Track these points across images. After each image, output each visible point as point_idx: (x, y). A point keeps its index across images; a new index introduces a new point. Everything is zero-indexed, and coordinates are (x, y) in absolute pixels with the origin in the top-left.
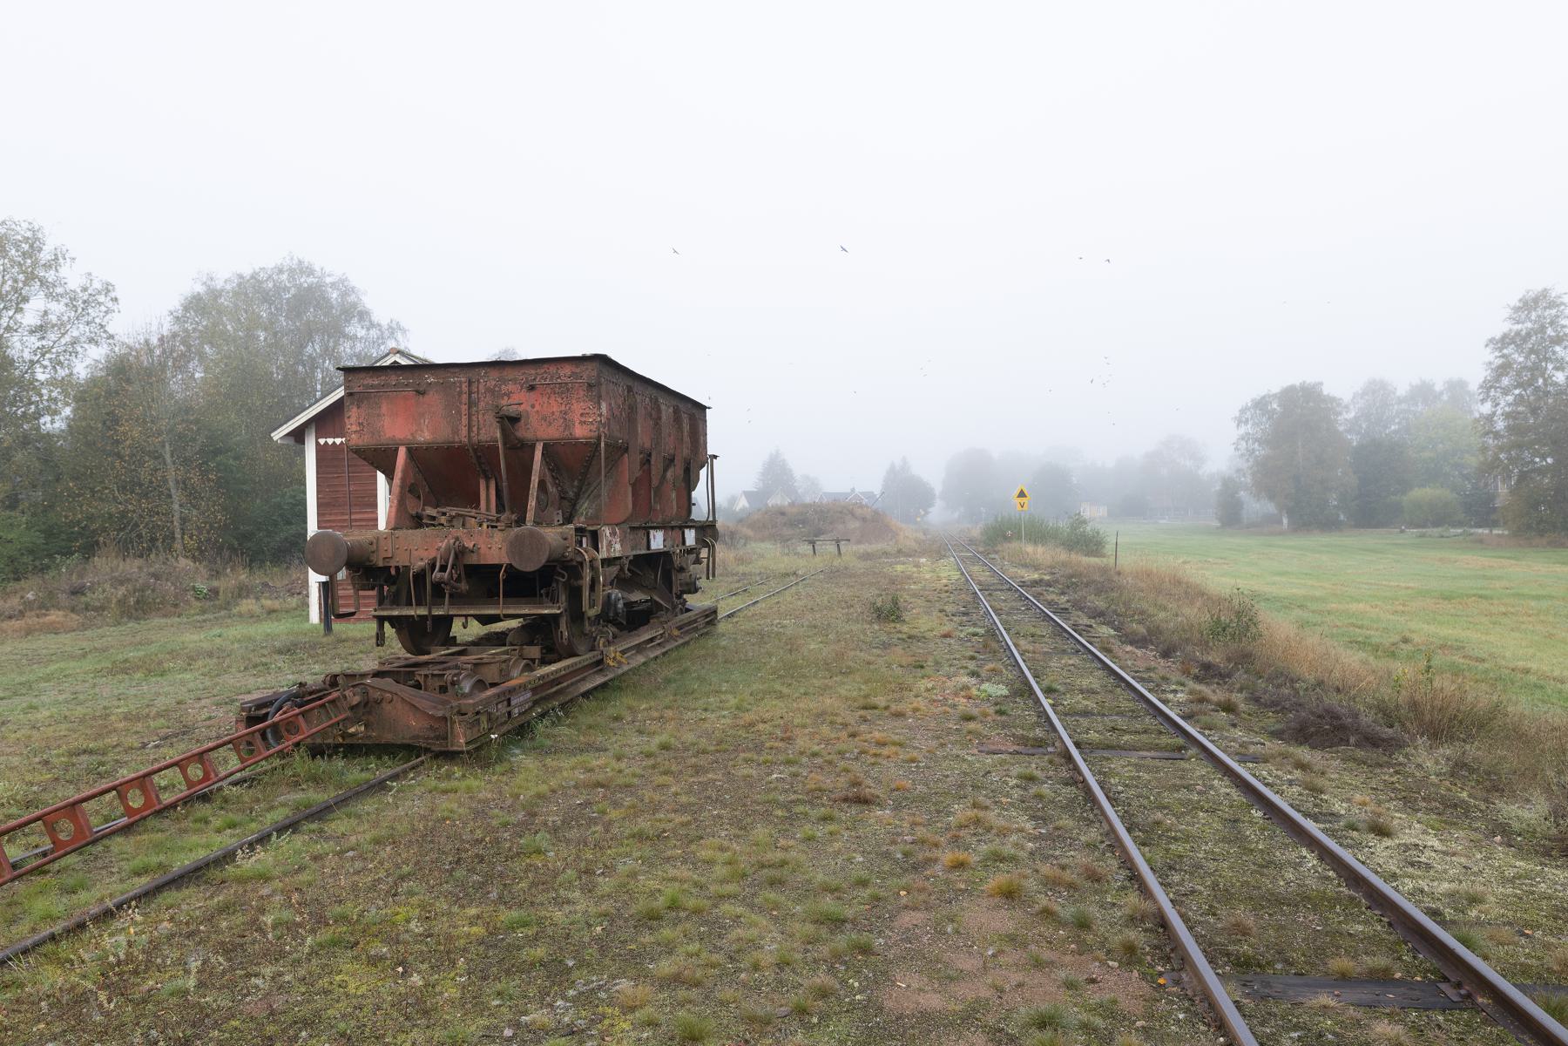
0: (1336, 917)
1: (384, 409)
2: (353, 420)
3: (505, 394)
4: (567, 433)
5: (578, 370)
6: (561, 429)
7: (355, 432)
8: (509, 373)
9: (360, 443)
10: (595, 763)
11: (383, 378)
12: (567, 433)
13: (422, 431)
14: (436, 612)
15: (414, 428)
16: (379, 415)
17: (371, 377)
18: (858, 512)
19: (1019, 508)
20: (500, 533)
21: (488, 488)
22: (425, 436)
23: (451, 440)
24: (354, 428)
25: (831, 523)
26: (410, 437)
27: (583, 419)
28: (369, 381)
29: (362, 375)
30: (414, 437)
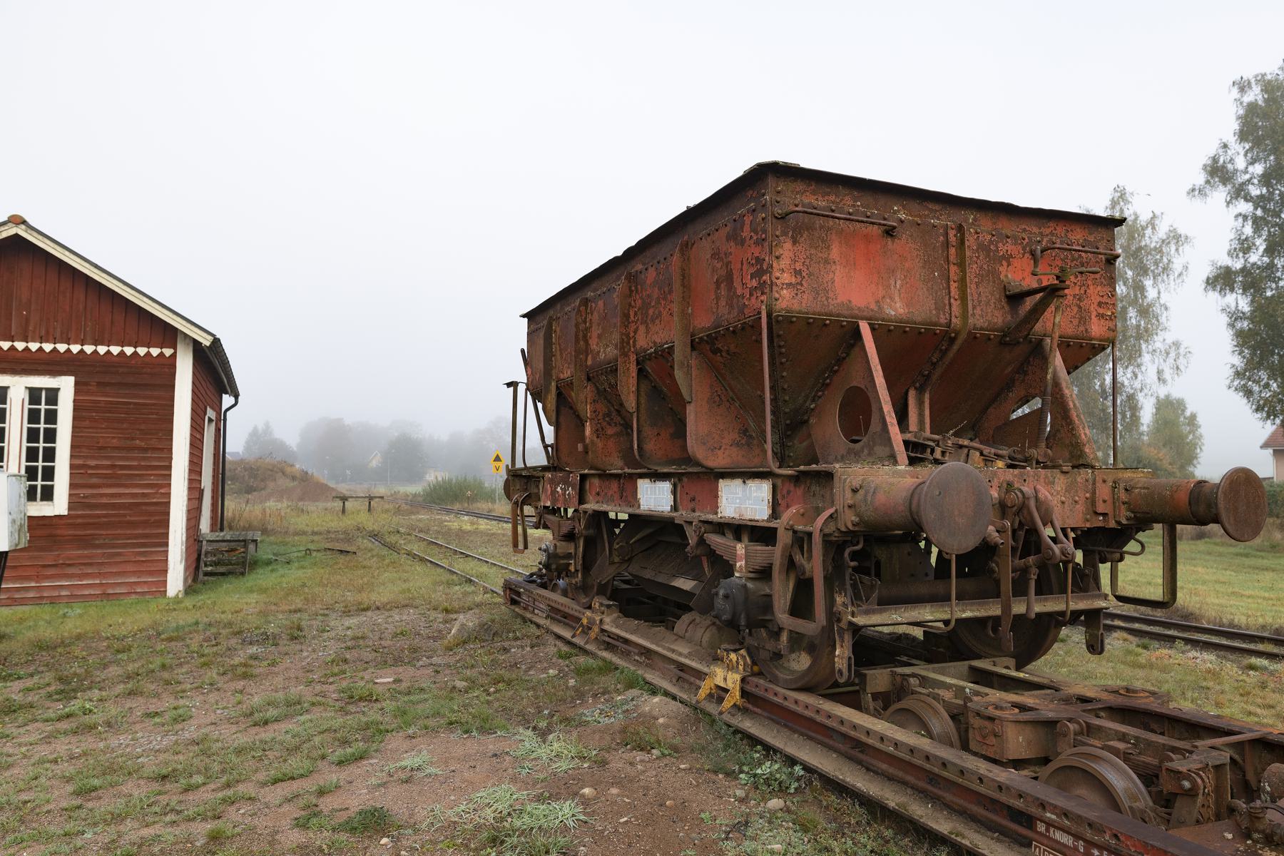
0: (574, 659)
1: (835, 252)
2: (784, 263)
3: (1003, 257)
4: (1082, 328)
5: (1091, 238)
6: (1076, 322)
7: (789, 285)
8: (1008, 226)
9: (796, 307)
10: (17, 596)
11: (833, 198)
12: (1082, 328)
13: (892, 299)
14: (1019, 608)
15: (881, 293)
16: (827, 262)
17: (814, 193)
18: (288, 470)
19: (494, 470)
20: (1062, 477)
21: (920, 403)
22: (896, 309)
23: (934, 319)
24: (786, 278)
25: (262, 480)
26: (873, 306)
27: (1101, 311)
28: (809, 199)
29: (800, 186)
30: (880, 308)
